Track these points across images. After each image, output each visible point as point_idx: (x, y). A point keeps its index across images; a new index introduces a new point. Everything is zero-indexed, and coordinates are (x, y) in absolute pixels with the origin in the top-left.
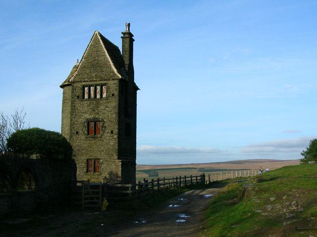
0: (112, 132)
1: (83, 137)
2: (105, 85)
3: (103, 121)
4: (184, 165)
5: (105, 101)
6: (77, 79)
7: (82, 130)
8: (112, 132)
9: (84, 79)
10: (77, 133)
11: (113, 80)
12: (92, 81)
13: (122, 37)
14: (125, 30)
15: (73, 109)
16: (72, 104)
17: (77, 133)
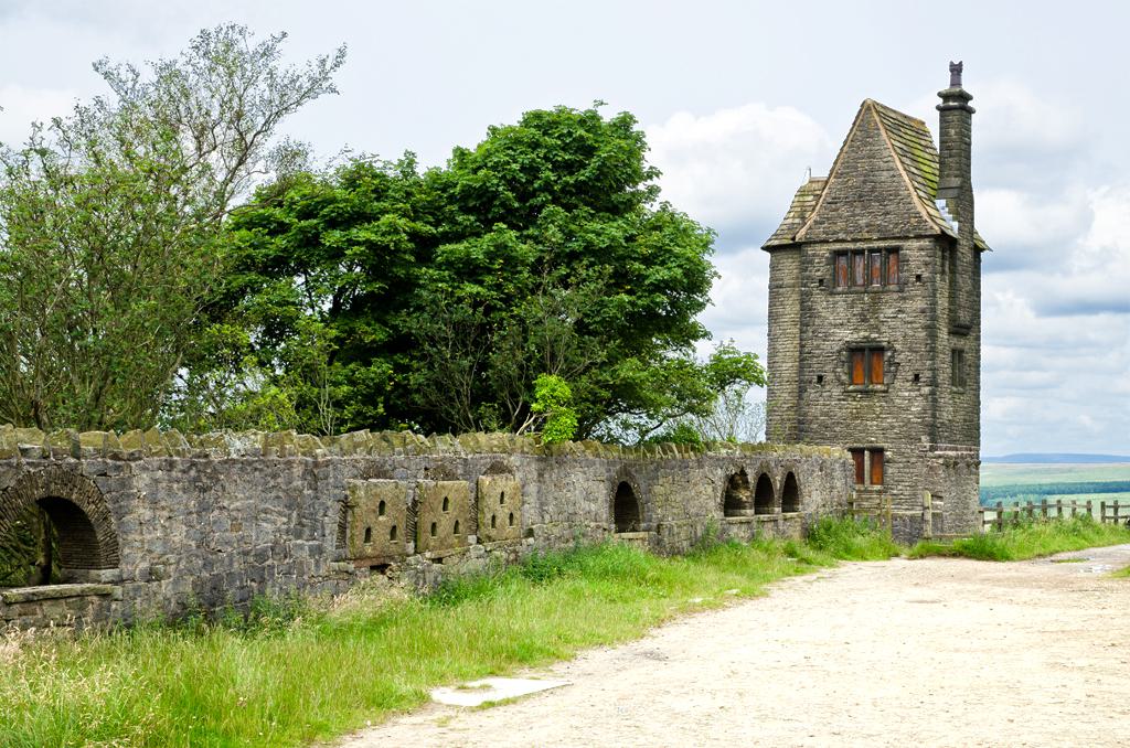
0: (917, 378)
1: (836, 392)
2: (896, 250)
3: (891, 348)
4: (895, 112)
5: (895, 296)
6: (819, 233)
7: (834, 371)
8: (917, 378)
9: (835, 233)
10: (820, 379)
11: (919, 237)
12: (860, 240)
13: (938, 108)
14: (945, 86)
15: (807, 313)
16: (802, 302)
17: (820, 379)
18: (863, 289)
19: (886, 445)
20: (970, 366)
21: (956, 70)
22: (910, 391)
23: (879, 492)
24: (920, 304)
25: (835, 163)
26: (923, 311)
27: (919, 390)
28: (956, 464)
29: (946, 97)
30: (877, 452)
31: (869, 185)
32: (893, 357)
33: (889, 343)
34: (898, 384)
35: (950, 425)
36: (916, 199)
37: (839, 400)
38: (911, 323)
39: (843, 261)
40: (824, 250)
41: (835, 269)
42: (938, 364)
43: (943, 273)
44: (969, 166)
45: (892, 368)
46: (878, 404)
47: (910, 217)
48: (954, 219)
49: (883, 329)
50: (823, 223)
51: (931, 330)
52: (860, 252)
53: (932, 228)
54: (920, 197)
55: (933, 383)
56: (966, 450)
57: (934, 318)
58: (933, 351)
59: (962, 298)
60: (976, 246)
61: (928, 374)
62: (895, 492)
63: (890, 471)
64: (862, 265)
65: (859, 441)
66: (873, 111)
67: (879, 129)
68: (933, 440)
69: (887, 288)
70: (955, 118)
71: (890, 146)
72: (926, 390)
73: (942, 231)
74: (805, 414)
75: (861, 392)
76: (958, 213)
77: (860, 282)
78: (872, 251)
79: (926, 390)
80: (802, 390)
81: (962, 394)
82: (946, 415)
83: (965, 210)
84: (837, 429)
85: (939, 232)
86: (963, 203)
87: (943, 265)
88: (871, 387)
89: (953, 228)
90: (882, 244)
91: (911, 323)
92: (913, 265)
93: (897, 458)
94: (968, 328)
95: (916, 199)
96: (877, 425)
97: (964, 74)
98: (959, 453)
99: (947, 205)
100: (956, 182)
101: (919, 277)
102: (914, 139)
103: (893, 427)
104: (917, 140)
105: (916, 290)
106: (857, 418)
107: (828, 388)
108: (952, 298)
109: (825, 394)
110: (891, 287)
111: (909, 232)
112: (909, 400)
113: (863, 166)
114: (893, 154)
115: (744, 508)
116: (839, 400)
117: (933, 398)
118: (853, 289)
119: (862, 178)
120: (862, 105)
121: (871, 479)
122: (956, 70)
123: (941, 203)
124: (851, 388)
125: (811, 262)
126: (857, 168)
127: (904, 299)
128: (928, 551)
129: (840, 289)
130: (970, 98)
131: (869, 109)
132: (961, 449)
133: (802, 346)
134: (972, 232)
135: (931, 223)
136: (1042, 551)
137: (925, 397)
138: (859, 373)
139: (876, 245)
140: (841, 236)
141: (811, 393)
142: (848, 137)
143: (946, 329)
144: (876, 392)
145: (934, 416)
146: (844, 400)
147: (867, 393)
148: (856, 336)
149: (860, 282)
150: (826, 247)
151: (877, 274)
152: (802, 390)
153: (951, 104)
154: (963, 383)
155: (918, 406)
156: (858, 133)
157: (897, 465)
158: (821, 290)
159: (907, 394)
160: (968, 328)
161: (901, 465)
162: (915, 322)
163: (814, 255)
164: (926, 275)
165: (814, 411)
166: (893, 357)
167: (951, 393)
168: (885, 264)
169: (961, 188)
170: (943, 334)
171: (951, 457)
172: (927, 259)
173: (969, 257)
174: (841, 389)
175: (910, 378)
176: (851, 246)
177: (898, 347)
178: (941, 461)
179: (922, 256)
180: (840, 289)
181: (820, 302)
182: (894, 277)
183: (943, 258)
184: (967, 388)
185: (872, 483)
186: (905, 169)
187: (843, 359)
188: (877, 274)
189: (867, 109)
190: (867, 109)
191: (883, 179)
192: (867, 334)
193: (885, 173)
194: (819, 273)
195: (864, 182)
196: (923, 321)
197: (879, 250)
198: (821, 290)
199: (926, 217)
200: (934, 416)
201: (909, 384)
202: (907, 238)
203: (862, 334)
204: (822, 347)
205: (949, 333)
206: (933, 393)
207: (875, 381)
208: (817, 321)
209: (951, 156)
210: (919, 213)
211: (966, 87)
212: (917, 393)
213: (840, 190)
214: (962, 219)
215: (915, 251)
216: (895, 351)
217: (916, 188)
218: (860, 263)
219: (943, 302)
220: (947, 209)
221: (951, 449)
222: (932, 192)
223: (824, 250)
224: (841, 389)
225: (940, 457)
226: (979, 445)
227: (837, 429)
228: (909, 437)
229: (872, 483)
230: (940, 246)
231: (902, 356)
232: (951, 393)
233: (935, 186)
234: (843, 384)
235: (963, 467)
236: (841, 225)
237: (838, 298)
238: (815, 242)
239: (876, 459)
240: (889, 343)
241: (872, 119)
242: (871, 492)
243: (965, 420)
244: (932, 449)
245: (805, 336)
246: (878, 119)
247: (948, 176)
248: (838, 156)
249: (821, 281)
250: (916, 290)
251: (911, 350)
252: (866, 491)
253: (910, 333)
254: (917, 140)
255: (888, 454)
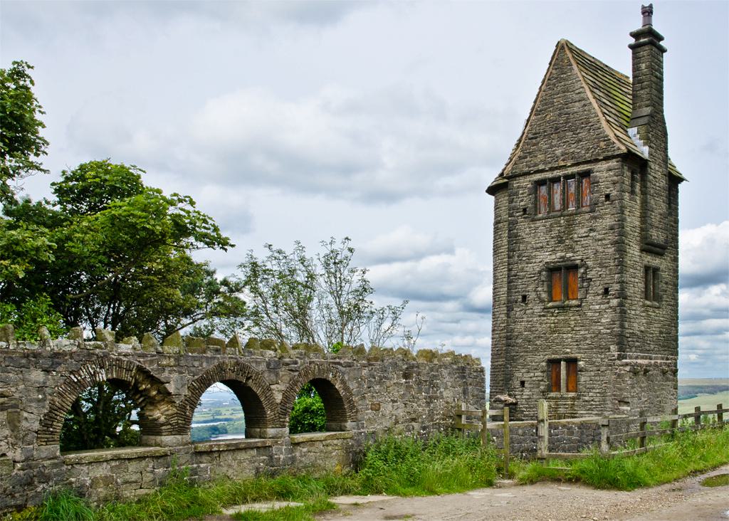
0: (606, 291)
1: (538, 309)
2: (586, 174)
3: (584, 265)
5: (587, 216)
7: (536, 291)
8: (606, 291)
9: (536, 165)
10: (524, 298)
11: (607, 159)
12: (556, 168)
13: (631, 47)
14: (638, 25)
17: (524, 298)
18: (559, 213)
19: (579, 356)
20: (666, 283)
21: (647, 12)
22: (600, 304)
23: (573, 399)
24: (609, 221)
25: (535, 102)
26: (612, 228)
27: (608, 303)
28: (646, 371)
29: (636, 35)
30: (572, 362)
31: (564, 117)
32: (585, 273)
33: (582, 260)
34: (590, 298)
35: (642, 337)
36: (604, 124)
37: (540, 316)
38: (601, 240)
39: (543, 190)
40: (526, 182)
41: (536, 197)
42: (627, 277)
43: (633, 192)
44: (661, 99)
45: (585, 284)
46: (572, 318)
47: (599, 141)
48: (645, 144)
49: (577, 248)
50: (526, 157)
51: (620, 247)
52: (556, 180)
53: (619, 149)
54: (608, 121)
55: (622, 295)
56: (663, 359)
57: (622, 234)
58: (621, 266)
59: (655, 218)
60: (670, 173)
61: (617, 287)
62: (587, 398)
63: (583, 379)
64: (559, 191)
65: (556, 353)
66: (566, 49)
67: (572, 65)
68: (621, 350)
69: (579, 210)
70: (645, 53)
71: (581, 78)
72: (615, 302)
73: (629, 151)
74: (512, 331)
75: (558, 307)
76: (648, 139)
77: (558, 206)
78: (567, 177)
79: (615, 302)
80: (510, 309)
81: (658, 308)
82: (637, 324)
83: (656, 138)
84: (538, 343)
85: (626, 151)
86: (656, 129)
87: (632, 186)
88: (567, 303)
89: (644, 151)
90: (575, 169)
91: (601, 240)
92: (602, 185)
93: (589, 367)
94: (664, 248)
95: (604, 124)
96: (572, 338)
97: (654, 17)
98: (653, 362)
99: (638, 133)
100: (647, 110)
101: (607, 197)
102: (612, 87)
103: (586, 339)
104: (618, 86)
105: (607, 210)
106: (554, 332)
107: (530, 306)
108: (644, 217)
109: (528, 312)
110: (584, 209)
111: (599, 155)
112: (599, 311)
113: (558, 101)
114: (584, 85)
115: (159, 433)
116: (540, 316)
117: (622, 313)
118: (552, 214)
119: (558, 112)
120: (557, 46)
121: (567, 387)
122: (647, 12)
123: (633, 131)
124: (550, 304)
125: (516, 194)
126: (553, 103)
127: (595, 218)
128: (540, 474)
129: (540, 216)
130: (661, 39)
131: (563, 48)
132: (656, 358)
133: (510, 270)
134: (666, 159)
135: (618, 144)
136: (701, 465)
137: (614, 309)
138: (558, 290)
139: (570, 171)
140: (541, 167)
141: (517, 311)
142: (545, 76)
143: (637, 247)
144: (571, 307)
145: (622, 326)
146: (544, 316)
147: (563, 308)
148: (554, 257)
149: (558, 206)
150: (528, 178)
151: (572, 198)
152: (510, 309)
153: (642, 40)
154: (657, 298)
155: (607, 318)
156: (554, 71)
157: (589, 374)
158: (524, 218)
159: (597, 307)
160: (664, 248)
161: (592, 373)
162: (604, 239)
163: (518, 187)
164: (614, 193)
165: (519, 327)
166: (585, 273)
167: (644, 306)
168: (579, 187)
169: (651, 116)
170: (634, 250)
171: (641, 365)
172: (615, 178)
173: (663, 183)
174: (541, 306)
175: (600, 292)
176: (549, 175)
177: (590, 263)
178: (628, 368)
179: (612, 176)
180: (540, 216)
181: (524, 228)
182: (587, 200)
183: (633, 179)
184: (664, 303)
185: (568, 391)
186: (595, 98)
187: (543, 278)
188: (572, 198)
189: (563, 48)
190: (563, 48)
191: (576, 109)
192: (563, 254)
193: (577, 104)
194: (522, 203)
195: (560, 115)
196: (612, 237)
197: (572, 176)
198: (524, 218)
199: (613, 139)
200: (622, 326)
201: (599, 297)
202: (597, 161)
203: (559, 254)
204: (525, 269)
205: (642, 250)
206: (621, 305)
207: (571, 297)
208: (522, 247)
209: (642, 89)
210: (607, 136)
211: (657, 27)
212: (607, 305)
213: (540, 125)
214: (652, 145)
215: (604, 172)
216: (588, 268)
217: (604, 114)
218: (558, 188)
219: (633, 221)
220: (638, 136)
221: (643, 358)
222: (625, 123)
223: (526, 182)
224: (541, 306)
225: (627, 364)
226: (677, 354)
227: (538, 343)
228: (599, 347)
229: (568, 391)
230: (629, 168)
231: (593, 273)
232: (644, 306)
233: (629, 115)
234: (542, 301)
235: (657, 375)
236: (541, 157)
237: (538, 224)
238: (520, 175)
239: (571, 368)
240: (582, 260)
241: (565, 56)
242: (566, 398)
243: (661, 332)
244: (620, 357)
245: (511, 260)
246: (570, 55)
247: (640, 107)
248: (538, 95)
249: (525, 210)
250: (607, 210)
251: (601, 265)
252: (562, 398)
253: (601, 249)
254: (618, 86)
255: (581, 363)
